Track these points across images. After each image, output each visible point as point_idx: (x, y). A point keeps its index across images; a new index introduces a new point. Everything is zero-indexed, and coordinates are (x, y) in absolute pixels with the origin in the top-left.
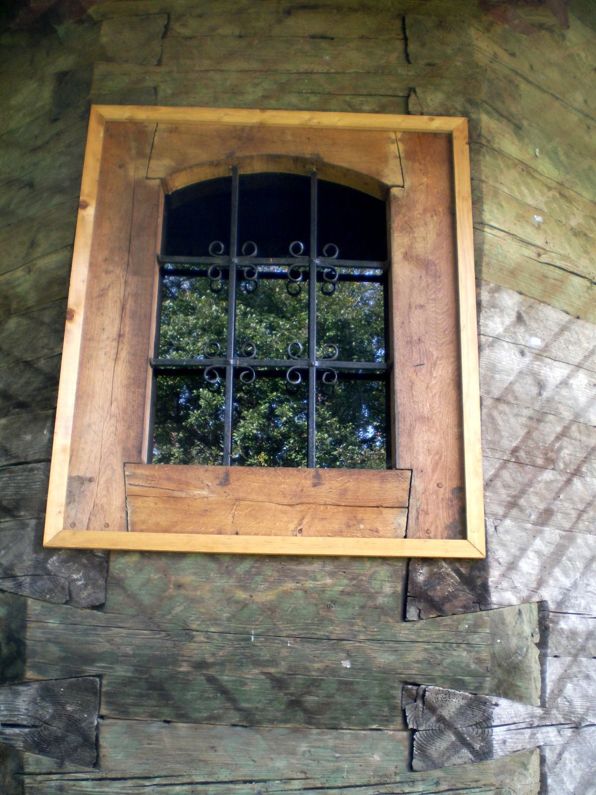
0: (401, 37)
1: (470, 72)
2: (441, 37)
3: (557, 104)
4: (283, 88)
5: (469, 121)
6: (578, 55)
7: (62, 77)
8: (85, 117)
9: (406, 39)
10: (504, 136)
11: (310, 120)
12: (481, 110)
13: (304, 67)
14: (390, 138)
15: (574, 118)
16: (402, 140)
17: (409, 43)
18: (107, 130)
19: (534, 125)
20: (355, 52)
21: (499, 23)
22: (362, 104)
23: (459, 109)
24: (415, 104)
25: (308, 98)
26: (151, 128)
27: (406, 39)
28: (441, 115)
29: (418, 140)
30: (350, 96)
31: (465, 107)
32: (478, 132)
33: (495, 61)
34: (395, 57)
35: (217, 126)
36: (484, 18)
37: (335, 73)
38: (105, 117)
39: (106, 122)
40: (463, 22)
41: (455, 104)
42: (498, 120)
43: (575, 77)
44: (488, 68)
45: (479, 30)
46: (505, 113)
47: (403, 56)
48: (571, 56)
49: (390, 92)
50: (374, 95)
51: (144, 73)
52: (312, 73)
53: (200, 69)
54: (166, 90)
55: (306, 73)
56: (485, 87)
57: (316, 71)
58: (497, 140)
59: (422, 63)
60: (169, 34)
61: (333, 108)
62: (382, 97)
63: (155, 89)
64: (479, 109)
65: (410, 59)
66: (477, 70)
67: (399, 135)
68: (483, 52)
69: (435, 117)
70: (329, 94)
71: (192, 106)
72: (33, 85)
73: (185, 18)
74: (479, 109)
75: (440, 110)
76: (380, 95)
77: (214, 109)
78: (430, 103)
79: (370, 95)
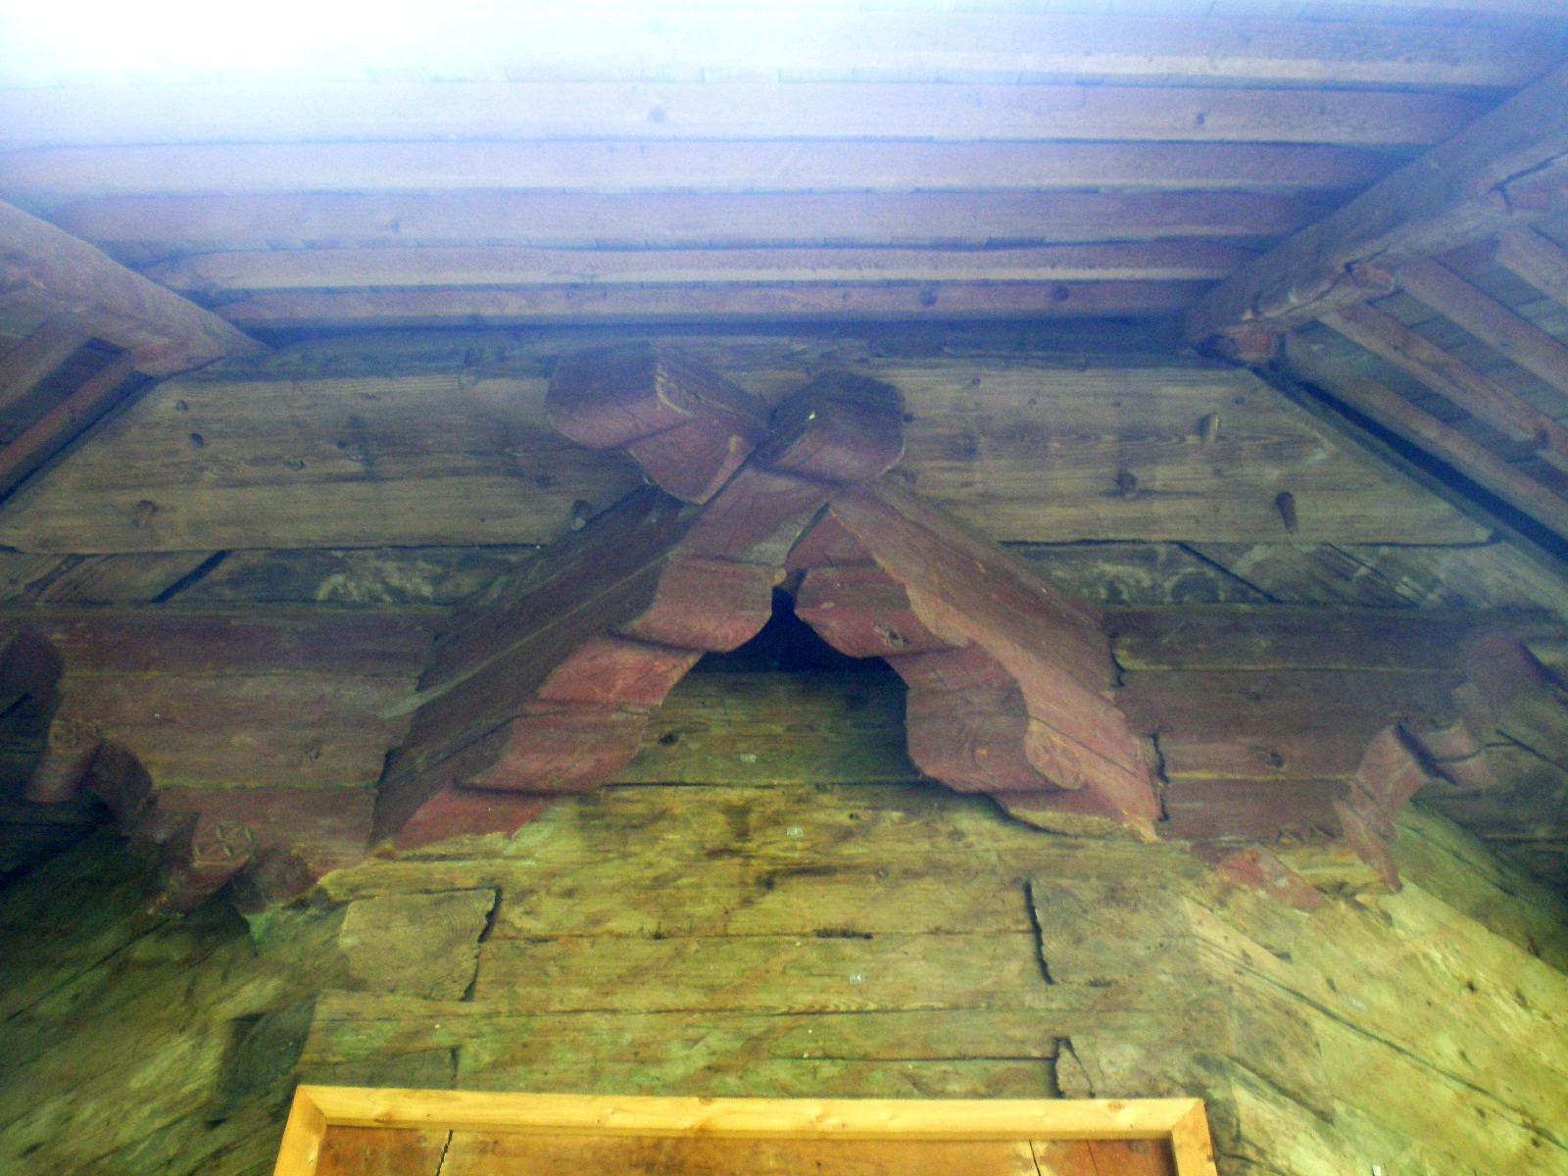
0: (1026, 925)
1: (1195, 996)
2: (1118, 922)
3: (1401, 1063)
4: (755, 1047)
5: (1207, 1107)
6: (1426, 956)
7: (245, 1024)
8: (279, 1115)
9: (1037, 930)
10: (1295, 1138)
11: (820, 1118)
12: (1232, 1079)
13: (803, 1000)
14: (1019, 1157)
15: (1446, 1092)
16: (1047, 1159)
17: (1044, 937)
18: (326, 1147)
19: (1359, 1112)
20: (922, 963)
21: (1245, 887)
22: (944, 1077)
23: (1181, 1081)
24: (1074, 1075)
25: (815, 1070)
26: (438, 1139)
27: (1037, 930)
28: (1138, 1095)
29: (1088, 1159)
30: (915, 1063)
31: (1194, 1076)
32: (1234, 1132)
33: (1248, 970)
34: (1016, 968)
35: (596, 1139)
36: (1210, 877)
37: (876, 1011)
38: (326, 1113)
39: (330, 1127)
40: (1164, 887)
41: (1168, 1069)
42: (1274, 1101)
43: (1429, 1004)
44: (1235, 986)
45: (1200, 904)
46: (1289, 1086)
47: (1034, 967)
48: (1411, 959)
49: (1011, 1050)
50: (975, 1058)
51: (431, 1017)
52: (822, 1012)
53: (561, 1008)
54: (478, 1053)
55: (810, 1012)
56: (1233, 1026)
57: (832, 1008)
58: (1279, 1148)
59: (1079, 979)
60: (496, 931)
61: (876, 1090)
62: (990, 1062)
63: (454, 1052)
64: (1226, 1078)
65: (1052, 975)
66: (1211, 989)
67: (1041, 1148)
68: (1214, 949)
69: (1125, 1101)
70: (866, 1058)
71: (538, 1089)
72: (182, 1044)
73: (535, 898)
74: (1226, 1078)
75: (1134, 1084)
76: (988, 1058)
77: (588, 1097)
78: (1109, 1070)
79: (963, 1058)
